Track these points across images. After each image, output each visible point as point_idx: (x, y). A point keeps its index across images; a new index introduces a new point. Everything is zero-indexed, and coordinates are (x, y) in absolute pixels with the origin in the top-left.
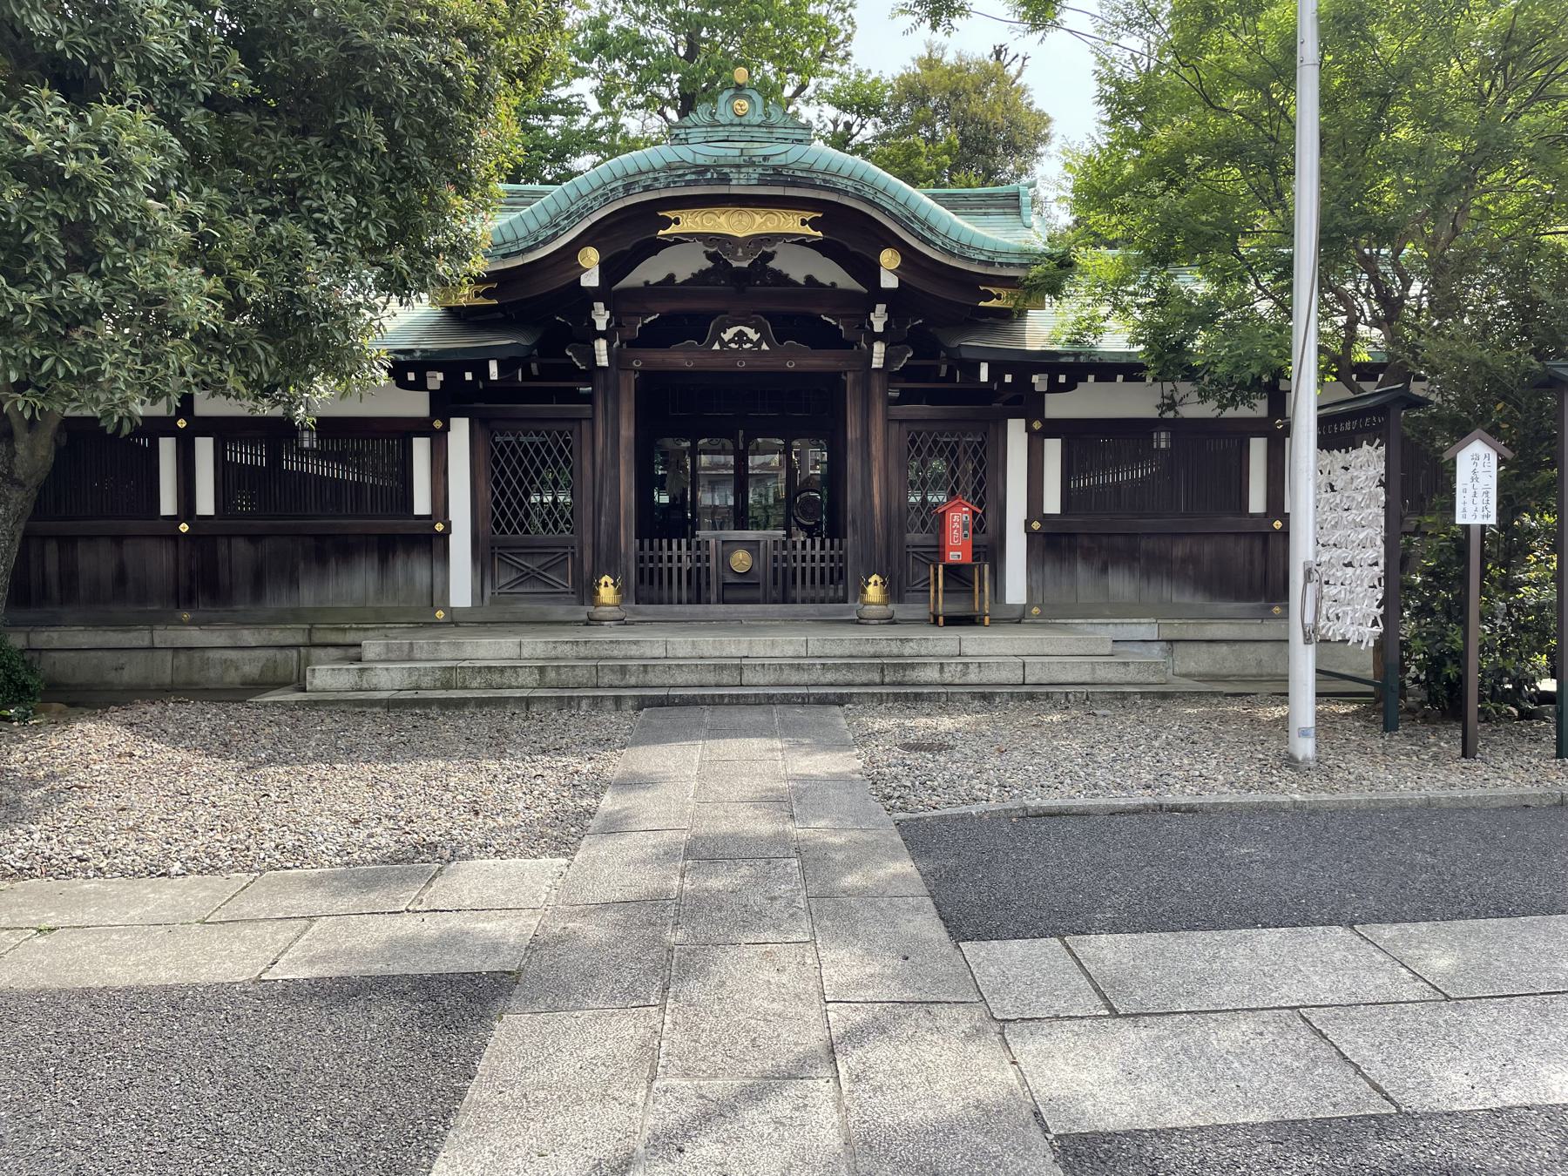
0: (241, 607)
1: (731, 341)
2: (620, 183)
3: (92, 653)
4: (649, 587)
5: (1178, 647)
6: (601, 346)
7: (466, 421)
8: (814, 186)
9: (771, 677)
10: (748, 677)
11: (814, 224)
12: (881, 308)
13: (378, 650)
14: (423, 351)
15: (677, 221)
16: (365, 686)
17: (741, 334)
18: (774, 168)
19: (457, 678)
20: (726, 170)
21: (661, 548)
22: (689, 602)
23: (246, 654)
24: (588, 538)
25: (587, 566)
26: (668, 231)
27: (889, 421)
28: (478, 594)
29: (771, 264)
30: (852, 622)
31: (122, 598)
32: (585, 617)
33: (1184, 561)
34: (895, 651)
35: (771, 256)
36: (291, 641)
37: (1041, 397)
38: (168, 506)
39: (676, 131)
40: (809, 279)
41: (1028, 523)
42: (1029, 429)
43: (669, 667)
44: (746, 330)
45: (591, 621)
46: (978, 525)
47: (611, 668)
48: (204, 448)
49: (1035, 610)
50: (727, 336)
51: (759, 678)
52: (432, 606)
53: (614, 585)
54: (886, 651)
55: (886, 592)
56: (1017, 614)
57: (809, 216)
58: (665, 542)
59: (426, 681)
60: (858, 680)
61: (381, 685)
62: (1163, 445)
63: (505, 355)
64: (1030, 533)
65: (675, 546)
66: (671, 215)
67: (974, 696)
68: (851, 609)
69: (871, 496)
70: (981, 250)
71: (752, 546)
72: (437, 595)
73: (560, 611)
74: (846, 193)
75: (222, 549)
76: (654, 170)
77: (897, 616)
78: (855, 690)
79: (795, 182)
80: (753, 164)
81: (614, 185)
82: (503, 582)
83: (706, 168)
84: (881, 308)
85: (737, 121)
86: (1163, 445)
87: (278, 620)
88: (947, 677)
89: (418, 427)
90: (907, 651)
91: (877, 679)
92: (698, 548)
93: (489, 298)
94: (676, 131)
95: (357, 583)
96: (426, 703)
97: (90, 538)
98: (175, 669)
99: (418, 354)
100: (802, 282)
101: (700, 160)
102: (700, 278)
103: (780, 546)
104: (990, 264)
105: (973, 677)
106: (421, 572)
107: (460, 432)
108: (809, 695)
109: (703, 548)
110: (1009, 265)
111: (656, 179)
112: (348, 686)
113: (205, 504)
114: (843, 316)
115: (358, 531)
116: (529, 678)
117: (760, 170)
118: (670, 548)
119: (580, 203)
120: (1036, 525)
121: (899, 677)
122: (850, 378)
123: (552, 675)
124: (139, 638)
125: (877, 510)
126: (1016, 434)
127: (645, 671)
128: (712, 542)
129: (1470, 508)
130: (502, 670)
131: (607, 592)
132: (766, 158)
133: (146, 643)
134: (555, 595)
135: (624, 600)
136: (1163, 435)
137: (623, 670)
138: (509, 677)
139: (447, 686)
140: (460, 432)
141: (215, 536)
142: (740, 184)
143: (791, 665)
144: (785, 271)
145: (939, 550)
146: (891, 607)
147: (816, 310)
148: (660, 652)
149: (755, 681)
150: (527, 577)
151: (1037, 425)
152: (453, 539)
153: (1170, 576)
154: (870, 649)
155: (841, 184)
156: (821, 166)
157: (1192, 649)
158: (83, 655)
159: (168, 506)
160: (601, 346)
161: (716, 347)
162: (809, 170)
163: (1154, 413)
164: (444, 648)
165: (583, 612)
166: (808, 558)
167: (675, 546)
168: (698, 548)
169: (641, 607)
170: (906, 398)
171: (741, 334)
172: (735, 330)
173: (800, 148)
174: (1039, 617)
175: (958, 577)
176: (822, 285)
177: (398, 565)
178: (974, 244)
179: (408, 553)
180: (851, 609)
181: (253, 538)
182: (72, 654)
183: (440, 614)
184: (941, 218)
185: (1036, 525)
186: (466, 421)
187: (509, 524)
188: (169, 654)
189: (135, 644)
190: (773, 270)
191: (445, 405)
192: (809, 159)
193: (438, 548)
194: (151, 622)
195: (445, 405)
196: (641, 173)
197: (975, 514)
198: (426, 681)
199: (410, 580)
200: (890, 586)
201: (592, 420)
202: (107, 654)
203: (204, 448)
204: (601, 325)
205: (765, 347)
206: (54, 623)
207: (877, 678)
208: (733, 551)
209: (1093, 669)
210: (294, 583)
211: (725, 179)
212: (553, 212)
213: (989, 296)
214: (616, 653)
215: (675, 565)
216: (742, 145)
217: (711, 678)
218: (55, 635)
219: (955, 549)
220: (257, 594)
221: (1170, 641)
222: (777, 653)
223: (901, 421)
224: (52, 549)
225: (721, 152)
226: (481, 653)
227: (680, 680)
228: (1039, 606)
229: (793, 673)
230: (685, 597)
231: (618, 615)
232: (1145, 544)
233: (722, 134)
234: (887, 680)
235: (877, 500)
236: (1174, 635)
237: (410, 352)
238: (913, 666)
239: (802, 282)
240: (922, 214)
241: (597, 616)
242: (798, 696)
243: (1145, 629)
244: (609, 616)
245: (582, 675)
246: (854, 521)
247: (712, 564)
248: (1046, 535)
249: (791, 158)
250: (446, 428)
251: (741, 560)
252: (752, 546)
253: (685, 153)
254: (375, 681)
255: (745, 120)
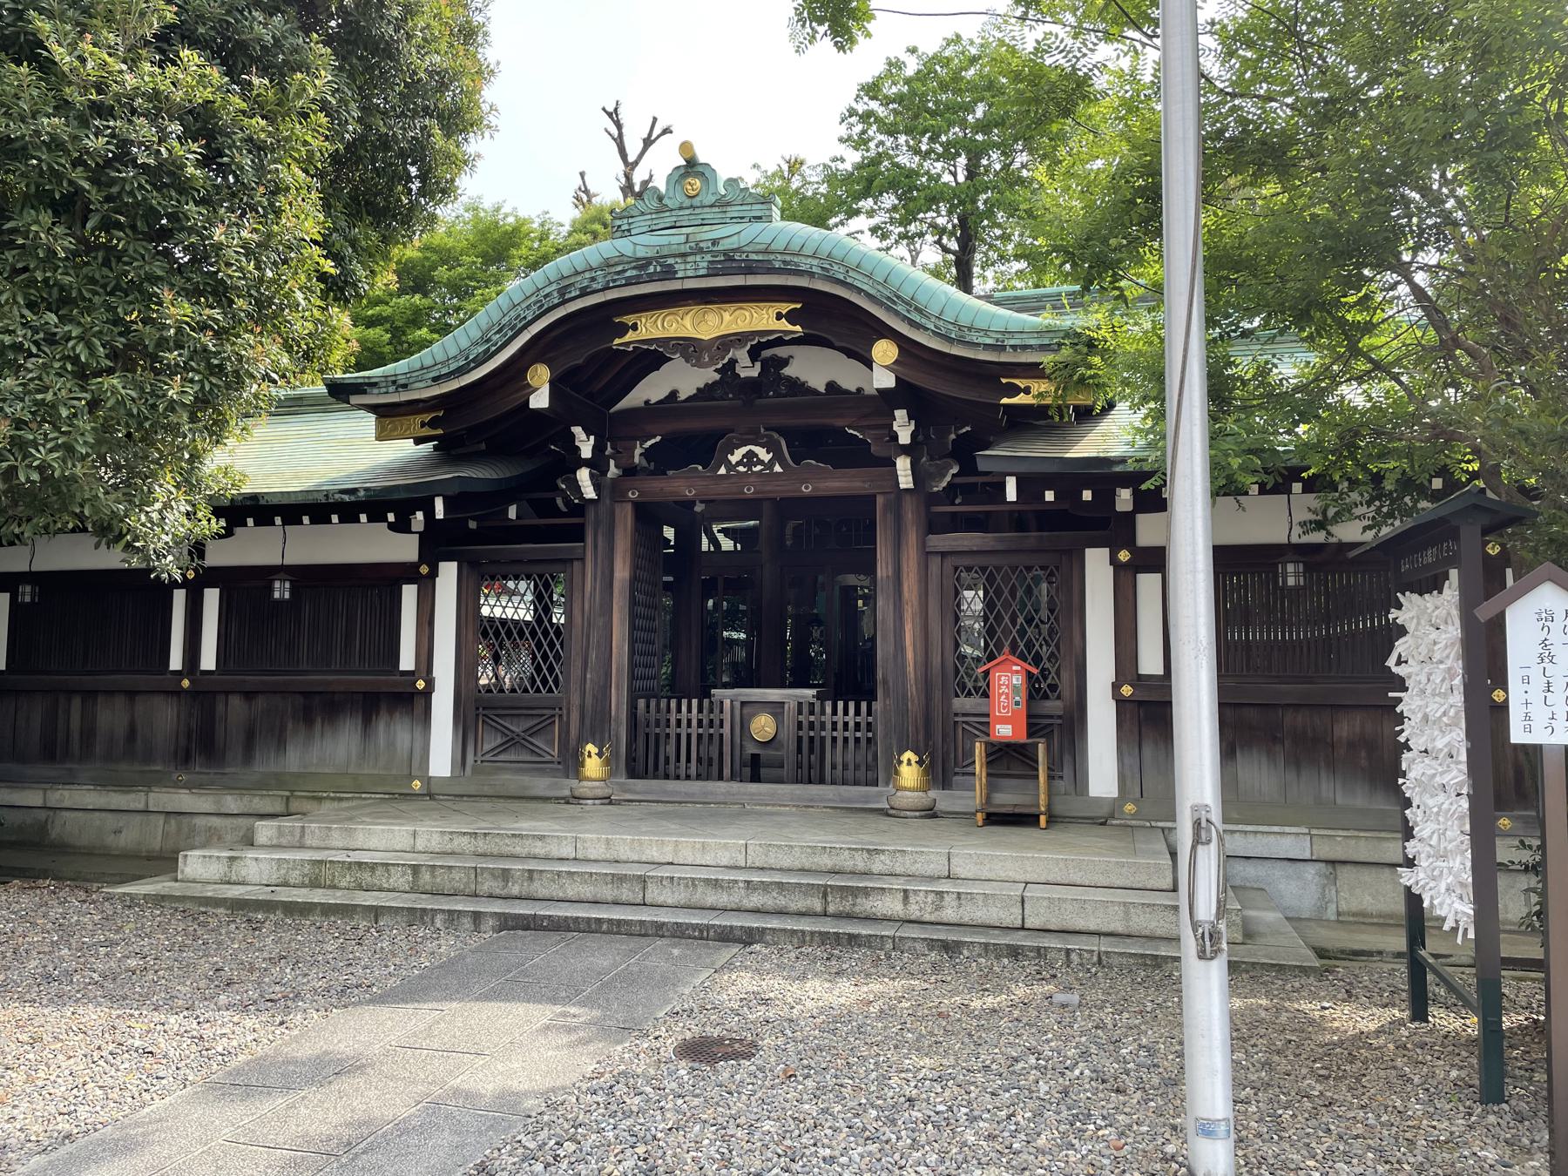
0: (232, 770)
1: (739, 463)
2: (554, 287)
3: (97, 814)
4: (644, 759)
5: (1345, 873)
6: (903, 464)
7: (455, 564)
8: (772, 271)
9: (681, 896)
10: (653, 894)
11: (791, 317)
12: (901, 415)
13: (269, 833)
14: (366, 489)
15: (635, 327)
16: (234, 878)
17: (750, 454)
18: (725, 253)
19: (326, 873)
20: (670, 261)
21: (669, 710)
22: (699, 777)
23: (228, 822)
24: (575, 700)
25: (574, 732)
26: (627, 338)
27: (926, 554)
28: (460, 760)
29: (787, 371)
30: (883, 813)
31: (130, 759)
32: (567, 793)
33: (1352, 745)
34: (861, 866)
35: (785, 362)
36: (270, 810)
37: (1129, 520)
38: (176, 662)
39: (618, 222)
40: (831, 386)
41: (1116, 687)
42: (1114, 561)
43: (559, 874)
44: (757, 449)
45: (574, 799)
46: (1036, 690)
47: (492, 872)
48: (212, 597)
49: (1129, 808)
50: (734, 459)
51: (667, 896)
52: (411, 778)
53: (600, 755)
54: (849, 864)
55: (926, 772)
56: (1104, 812)
57: (785, 308)
58: (673, 703)
59: (295, 876)
60: (793, 907)
61: (250, 878)
62: (1291, 581)
63: (454, 490)
64: (1121, 702)
65: (684, 708)
66: (629, 319)
67: (932, 944)
68: (880, 794)
69: (903, 649)
70: (986, 332)
71: (776, 709)
72: (415, 764)
73: (541, 784)
74: (811, 275)
75: (220, 707)
76: (592, 269)
77: (942, 806)
78: (774, 923)
79: (750, 270)
80: (701, 251)
81: (547, 290)
82: (487, 747)
83: (649, 261)
84: (901, 415)
85: (687, 203)
86: (1291, 581)
87: (262, 786)
88: (914, 911)
89: (407, 573)
90: (877, 867)
91: (818, 907)
92: (711, 711)
93: (434, 428)
94: (618, 222)
95: (339, 746)
96: (291, 908)
97: (110, 693)
98: (165, 835)
99: (362, 493)
100: (822, 389)
101: (641, 253)
102: (705, 392)
103: (805, 709)
104: (999, 348)
105: (949, 913)
106: (400, 732)
107: (448, 573)
108: (708, 927)
109: (717, 711)
110: (1025, 347)
111: (593, 279)
112: (217, 877)
113: (208, 661)
114: (869, 427)
115: (342, 689)
116: (401, 880)
117: (708, 257)
118: (679, 710)
119: (512, 314)
120: (1127, 691)
121: (846, 906)
122: (880, 500)
123: (426, 877)
124: (134, 800)
125: (910, 668)
126: (1098, 566)
127: (531, 879)
128: (727, 703)
129: (1540, 715)
130: (373, 867)
131: (593, 765)
132: (715, 242)
133: (141, 806)
134: (539, 766)
135: (612, 774)
136: (1290, 568)
137: (506, 875)
138: (380, 878)
139: (315, 884)
140: (448, 573)
141: (214, 693)
142: (690, 276)
143: (707, 881)
144: (803, 379)
145: (983, 723)
146: (932, 794)
147: (839, 423)
148: (567, 851)
149: (660, 900)
150: (511, 743)
151: (1124, 556)
152: (436, 698)
153: (1332, 766)
154: (826, 861)
155: (804, 264)
156: (779, 245)
157: (1367, 875)
158: (89, 815)
159: (176, 662)
160: (903, 464)
161: (722, 471)
162: (766, 252)
163: (1282, 539)
164: (336, 834)
165: (566, 786)
166: (840, 726)
167: (684, 708)
168: (711, 711)
169: (639, 784)
170: (934, 526)
171: (750, 454)
172: (744, 450)
173: (759, 226)
174: (1134, 816)
175: (1010, 760)
176: (847, 392)
177: (381, 726)
178: (978, 324)
179: (391, 713)
180: (880, 794)
181: (249, 695)
182: (80, 814)
183: (417, 784)
184: (933, 294)
185: (1127, 691)
186: (455, 564)
187: (545, 682)
188: (161, 819)
189: (132, 806)
190: (789, 378)
191: (436, 545)
192: (765, 239)
193: (419, 703)
194: (148, 782)
195: (436, 545)
196: (577, 273)
197: (1030, 675)
198: (295, 876)
199: (391, 745)
200: (932, 766)
201: (582, 560)
202: (109, 816)
203: (212, 597)
204: (586, 451)
205: (778, 469)
206: (69, 781)
207: (817, 906)
208: (754, 715)
209: (1127, 913)
210: (281, 744)
211: (669, 273)
212: (484, 327)
213: (1015, 391)
214: (518, 850)
215: (683, 731)
216: (684, 230)
217: (607, 892)
218: (66, 793)
219: (1004, 721)
220: (248, 757)
221: (1332, 863)
222: (708, 860)
223: (943, 554)
224: (76, 702)
225: (664, 241)
226: (373, 842)
227: (571, 893)
228: (1135, 802)
229: (709, 891)
230: (693, 771)
231: (600, 793)
232: (1289, 718)
233: (669, 221)
234: (831, 909)
235: (910, 655)
236: (1338, 853)
237: (353, 491)
238: (866, 892)
239: (822, 389)
240: (906, 293)
241: (577, 794)
242: (695, 927)
243: (1291, 842)
244: (589, 794)
245: (459, 879)
246: (885, 682)
247: (726, 730)
248: (1140, 703)
249: (744, 239)
250: (434, 574)
251: (763, 726)
252: (776, 709)
253: (624, 246)
254: (243, 873)
255: (696, 202)
